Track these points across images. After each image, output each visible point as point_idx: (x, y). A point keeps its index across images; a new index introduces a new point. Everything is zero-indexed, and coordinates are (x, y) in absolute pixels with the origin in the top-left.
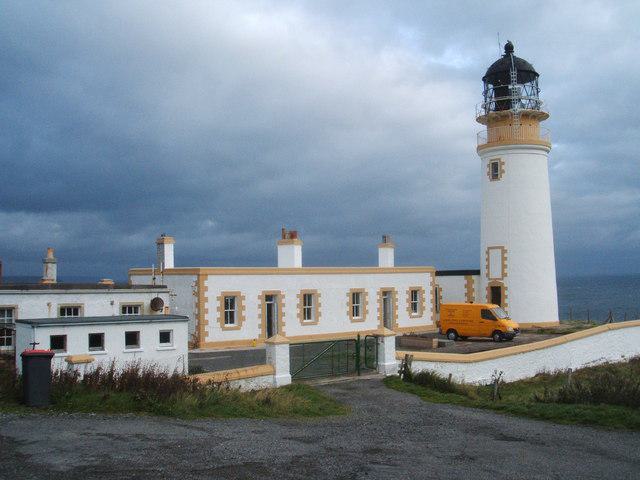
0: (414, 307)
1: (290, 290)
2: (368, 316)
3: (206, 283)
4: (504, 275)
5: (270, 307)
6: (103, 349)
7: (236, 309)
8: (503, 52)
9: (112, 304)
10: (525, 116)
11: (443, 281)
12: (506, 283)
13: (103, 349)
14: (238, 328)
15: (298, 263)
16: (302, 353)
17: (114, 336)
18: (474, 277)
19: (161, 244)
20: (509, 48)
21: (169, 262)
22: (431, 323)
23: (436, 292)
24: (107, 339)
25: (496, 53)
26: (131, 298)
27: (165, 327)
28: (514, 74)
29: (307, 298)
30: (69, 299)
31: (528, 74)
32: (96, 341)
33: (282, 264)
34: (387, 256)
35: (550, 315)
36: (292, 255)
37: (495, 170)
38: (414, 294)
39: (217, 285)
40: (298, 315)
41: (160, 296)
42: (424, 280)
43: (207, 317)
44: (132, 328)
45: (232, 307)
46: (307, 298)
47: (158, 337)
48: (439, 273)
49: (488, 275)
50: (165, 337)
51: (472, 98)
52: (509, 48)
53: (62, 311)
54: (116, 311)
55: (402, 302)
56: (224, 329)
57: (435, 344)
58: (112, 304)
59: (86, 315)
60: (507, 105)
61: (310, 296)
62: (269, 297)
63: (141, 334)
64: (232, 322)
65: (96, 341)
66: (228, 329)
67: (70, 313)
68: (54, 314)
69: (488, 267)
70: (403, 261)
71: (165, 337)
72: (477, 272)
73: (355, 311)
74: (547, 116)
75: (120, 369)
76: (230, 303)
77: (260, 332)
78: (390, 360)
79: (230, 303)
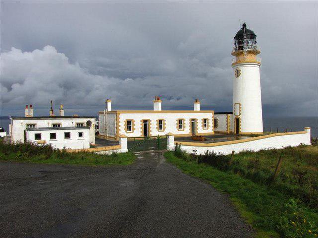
0: (205, 126)
1: (153, 118)
2: (135, 131)
3: (120, 116)
4: (241, 114)
5: (145, 126)
6: (55, 139)
7: (163, 125)
8: (242, 27)
9: (72, 123)
10: (250, 52)
11: (219, 117)
12: (241, 117)
13: (55, 139)
14: (132, 133)
15: (160, 109)
16: (131, 143)
17: (74, 134)
18: (229, 115)
19: (107, 102)
20: (245, 26)
21: (109, 109)
22: (212, 132)
23: (215, 120)
24: (57, 135)
25: (239, 28)
26: (80, 121)
27: (81, 131)
28: (245, 35)
29: (160, 122)
30: (56, 121)
31: (253, 36)
32: (67, 136)
33: (155, 109)
34: (197, 106)
35: (259, 129)
36: (158, 106)
37: (238, 74)
38: (205, 121)
39: (124, 117)
40: (202, 126)
41: (91, 120)
42: (209, 116)
43: (120, 128)
44: (81, 131)
45: (130, 125)
46: (160, 122)
47: (57, 137)
48: (215, 113)
49: (234, 114)
50: (81, 135)
51: (231, 44)
52: (245, 26)
53: (54, 125)
54: (50, 126)
55: (200, 124)
56: (127, 133)
57: (204, 140)
58: (72, 123)
59: (37, 127)
60: (242, 48)
61: (162, 121)
62: (145, 121)
63: (71, 134)
64: (130, 130)
65: (67, 136)
66: (129, 133)
67: (56, 126)
68: (50, 126)
69: (235, 111)
70: (203, 108)
71: (81, 135)
72: (231, 113)
73: (180, 127)
74: (232, 54)
75: (61, 148)
76: (129, 124)
77: (190, 131)
78: (172, 145)
79: (129, 124)
